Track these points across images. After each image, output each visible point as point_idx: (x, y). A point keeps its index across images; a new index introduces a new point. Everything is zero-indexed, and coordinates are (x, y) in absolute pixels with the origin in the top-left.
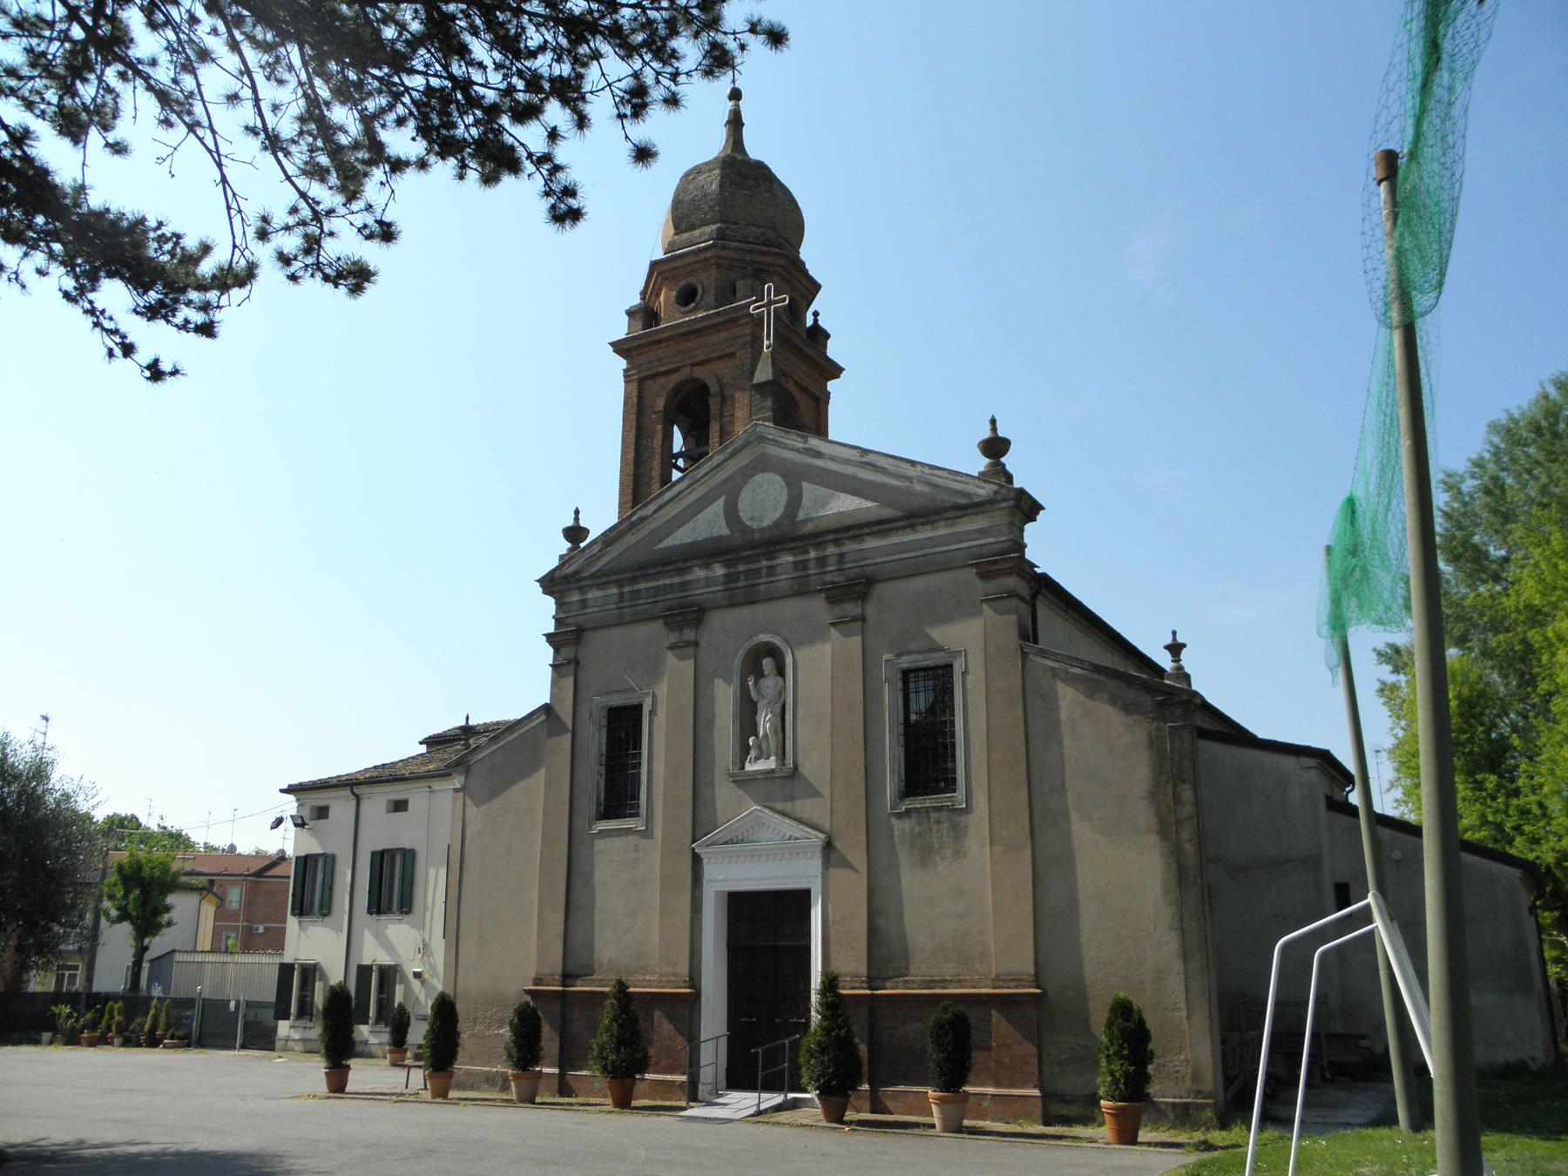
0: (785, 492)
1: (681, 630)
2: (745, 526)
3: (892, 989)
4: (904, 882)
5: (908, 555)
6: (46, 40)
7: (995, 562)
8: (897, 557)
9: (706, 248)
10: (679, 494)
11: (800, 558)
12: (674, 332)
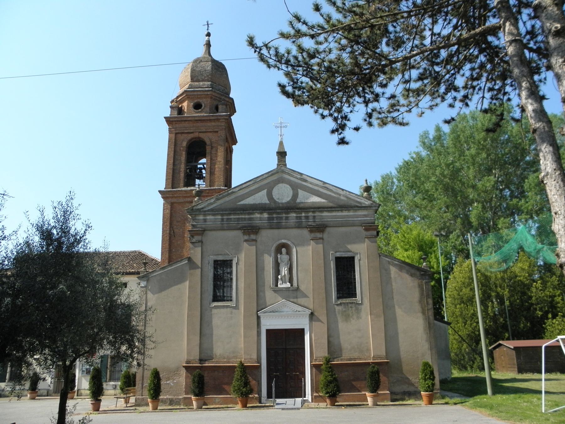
0: (292, 192)
1: (249, 235)
4: (340, 327)
6: (442, 35)
7: (371, 226)
8: (336, 220)
9: (208, 91)
10: (249, 185)
12: (193, 119)
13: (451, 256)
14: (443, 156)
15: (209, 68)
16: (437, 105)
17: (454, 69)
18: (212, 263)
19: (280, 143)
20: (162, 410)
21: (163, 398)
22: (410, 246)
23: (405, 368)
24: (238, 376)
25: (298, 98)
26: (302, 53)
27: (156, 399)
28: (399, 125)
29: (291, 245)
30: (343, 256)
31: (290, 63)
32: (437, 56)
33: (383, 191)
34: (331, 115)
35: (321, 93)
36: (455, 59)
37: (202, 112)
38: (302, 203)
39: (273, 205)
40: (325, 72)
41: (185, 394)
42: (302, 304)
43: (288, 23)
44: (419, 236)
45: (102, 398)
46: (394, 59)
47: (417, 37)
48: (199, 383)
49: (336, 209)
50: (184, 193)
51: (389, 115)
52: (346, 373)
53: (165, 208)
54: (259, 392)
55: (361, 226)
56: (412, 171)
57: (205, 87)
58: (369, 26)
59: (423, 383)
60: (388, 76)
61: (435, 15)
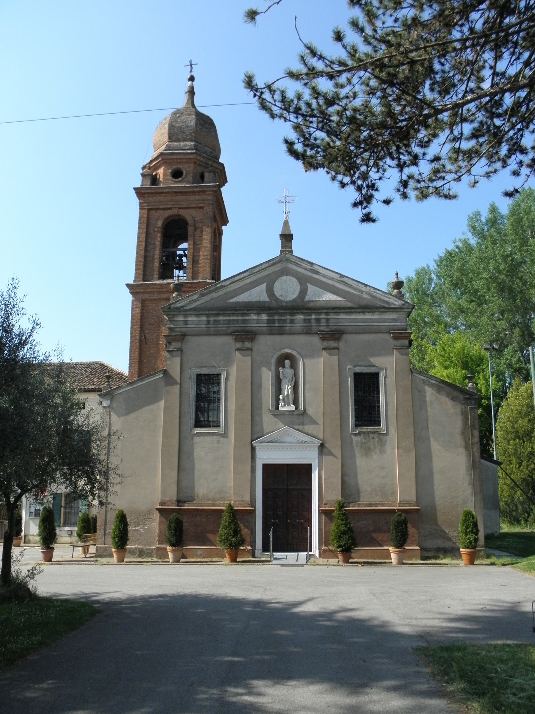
1: (243, 342)
2: (277, 299)
3: (353, 507)
5: (361, 324)
6: (507, 75)
7: (402, 333)
8: (356, 324)
9: (191, 153)
10: (243, 278)
11: (307, 318)
12: (171, 190)
13: (505, 377)
14: (498, 245)
15: (193, 123)
16: (495, 171)
17: (521, 122)
18: (194, 378)
19: (284, 223)
20: (130, 562)
21: (130, 548)
22: (452, 362)
23: (440, 517)
24: (226, 522)
25: (311, 160)
26: (316, 98)
27: (122, 548)
28: (443, 198)
29: (297, 356)
30: (365, 371)
31: (300, 112)
32: (499, 104)
33: (417, 290)
34: (353, 182)
35: (341, 153)
36: (524, 109)
37: (183, 182)
38: (312, 301)
39: (274, 304)
40: (348, 124)
41: (159, 544)
42: (310, 432)
43: (298, 58)
44: (464, 350)
45: (55, 546)
46: (440, 107)
47: (473, 78)
48: (176, 531)
49: (357, 310)
50: (159, 287)
51: (431, 185)
52: (365, 522)
53: (134, 306)
54: (253, 544)
55: (389, 333)
56: (457, 265)
57: (186, 148)
58: (408, 63)
59: (464, 537)
60: (431, 132)
61: (500, 47)
